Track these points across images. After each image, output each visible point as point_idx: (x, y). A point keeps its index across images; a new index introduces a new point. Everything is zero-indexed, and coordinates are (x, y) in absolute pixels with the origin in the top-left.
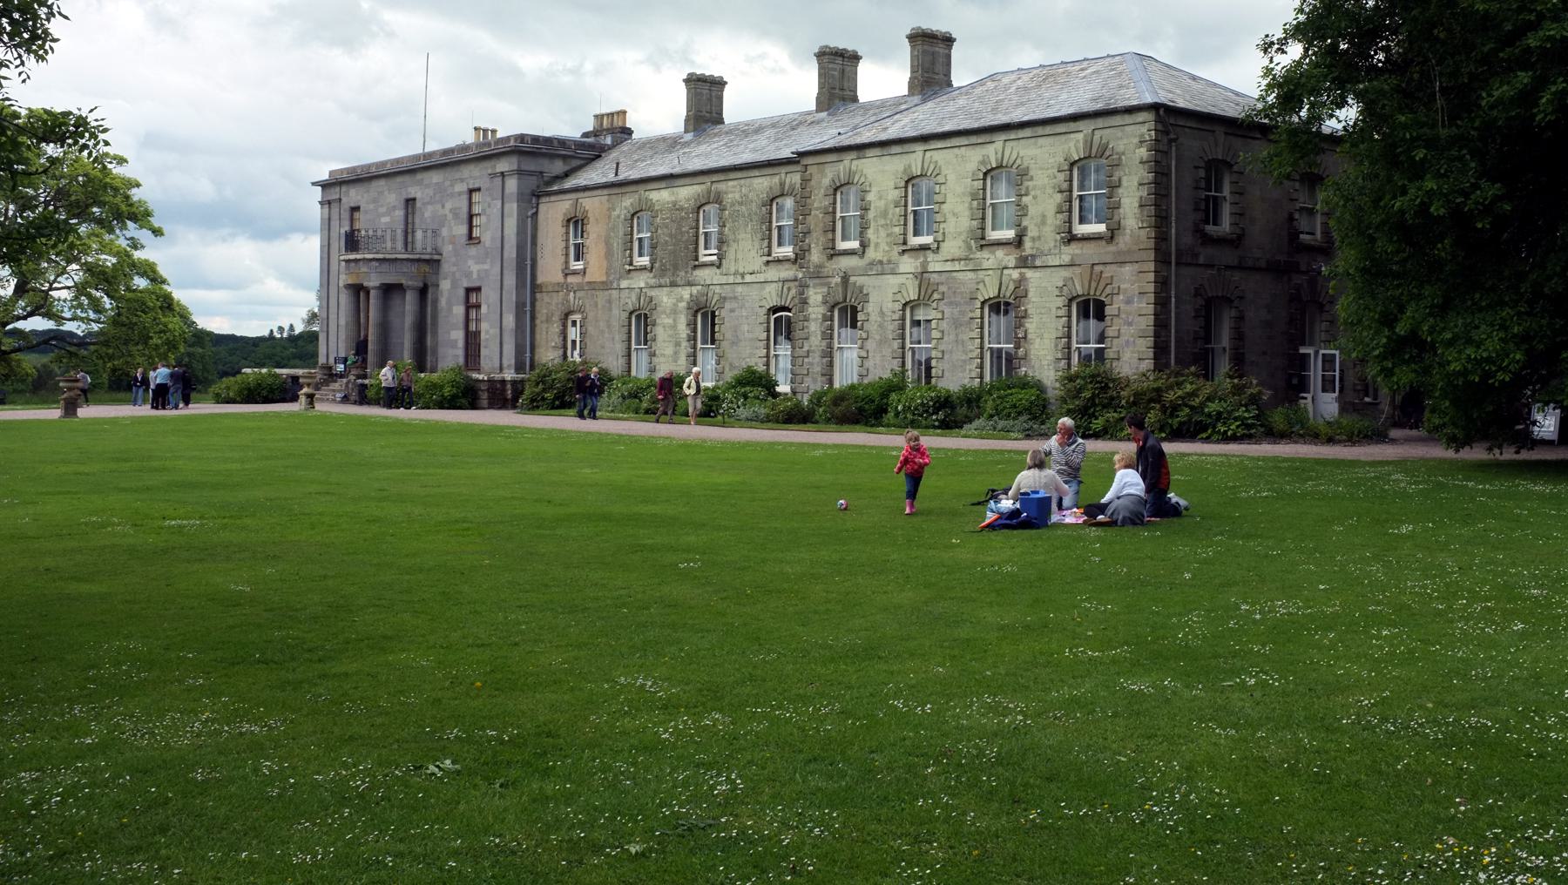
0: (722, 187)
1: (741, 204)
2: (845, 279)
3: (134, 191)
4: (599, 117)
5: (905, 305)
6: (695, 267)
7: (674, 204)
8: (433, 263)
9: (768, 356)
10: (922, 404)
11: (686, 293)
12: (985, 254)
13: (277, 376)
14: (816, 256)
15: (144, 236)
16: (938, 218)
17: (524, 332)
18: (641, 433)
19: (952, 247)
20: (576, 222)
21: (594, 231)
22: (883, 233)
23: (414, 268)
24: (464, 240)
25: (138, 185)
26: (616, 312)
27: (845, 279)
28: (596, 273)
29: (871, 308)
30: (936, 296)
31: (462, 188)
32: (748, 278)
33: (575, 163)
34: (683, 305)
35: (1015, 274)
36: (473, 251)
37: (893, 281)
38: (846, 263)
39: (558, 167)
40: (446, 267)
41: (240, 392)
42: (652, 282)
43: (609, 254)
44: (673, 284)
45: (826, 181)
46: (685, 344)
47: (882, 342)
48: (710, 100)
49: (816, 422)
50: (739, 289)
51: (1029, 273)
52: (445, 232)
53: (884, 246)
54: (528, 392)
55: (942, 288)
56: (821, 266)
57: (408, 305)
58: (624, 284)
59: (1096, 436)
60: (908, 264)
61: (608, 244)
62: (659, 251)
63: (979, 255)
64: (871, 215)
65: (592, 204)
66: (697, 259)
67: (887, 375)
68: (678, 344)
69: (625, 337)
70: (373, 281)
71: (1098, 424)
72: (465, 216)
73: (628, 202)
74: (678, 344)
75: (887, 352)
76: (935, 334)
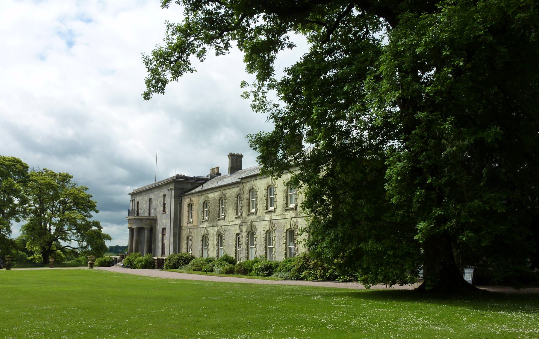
0: (225, 191)
1: (230, 197)
2: (252, 223)
3: (90, 199)
4: (212, 170)
5: (267, 232)
6: (218, 220)
7: (214, 197)
8: (155, 220)
9: (236, 251)
10: (261, 267)
11: (216, 229)
12: (287, 213)
13: (111, 258)
14: (244, 215)
15: (92, 213)
16: (275, 200)
17: (176, 243)
18: (269, 283)
19: (279, 211)
20: (190, 205)
21: (195, 207)
22: (261, 206)
23: (148, 222)
24: (162, 212)
25: (91, 196)
26: (199, 236)
27: (252, 223)
28: (195, 223)
29: (258, 233)
30: (274, 228)
31: (162, 194)
32: (231, 223)
33: (196, 185)
34: (215, 233)
35: (295, 220)
36: (164, 216)
37: (263, 223)
38: (252, 217)
39: (189, 186)
40: (159, 221)
41: (99, 264)
42: (208, 225)
43: (198, 215)
44: (213, 226)
45: (247, 188)
46: (216, 247)
47: (260, 245)
48: (237, 162)
49: (234, 274)
50: (229, 227)
51: (299, 219)
52: (158, 209)
53: (261, 211)
54: (166, 263)
55: (276, 226)
56: (245, 218)
57: (146, 234)
58: (201, 226)
59: (302, 279)
60: (267, 217)
61: (198, 212)
62: (210, 215)
63: (285, 213)
64: (258, 199)
65: (195, 199)
66: (219, 217)
67: (19, 235)
68: (214, 247)
69: (201, 244)
70: (134, 227)
71: (302, 275)
72: (162, 204)
73: (203, 198)
74: (214, 247)
75: (262, 249)
76: (274, 242)
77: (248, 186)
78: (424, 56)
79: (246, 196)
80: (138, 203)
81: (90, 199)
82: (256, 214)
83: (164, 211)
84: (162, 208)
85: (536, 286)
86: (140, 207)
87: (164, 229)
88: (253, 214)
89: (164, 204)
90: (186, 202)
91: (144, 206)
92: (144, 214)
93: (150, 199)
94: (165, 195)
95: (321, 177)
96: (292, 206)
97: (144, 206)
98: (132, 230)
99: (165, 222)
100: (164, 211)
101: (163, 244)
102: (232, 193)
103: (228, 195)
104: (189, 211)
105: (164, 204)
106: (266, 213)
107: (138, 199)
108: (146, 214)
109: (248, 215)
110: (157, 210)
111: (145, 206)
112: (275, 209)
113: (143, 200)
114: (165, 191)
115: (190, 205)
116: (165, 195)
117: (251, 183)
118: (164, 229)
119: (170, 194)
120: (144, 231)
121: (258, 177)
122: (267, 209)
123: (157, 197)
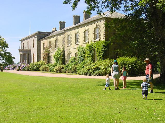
3: (6, 43)
6: (55, 49)
8: (30, 51)
31: (32, 40)
39: (43, 36)
77: (67, 34)
78: (145, 10)
79: (66, 38)
80: (23, 44)
81: (6, 43)
82: (71, 46)
83: (33, 46)
84: (33, 46)
85: (164, 89)
86: (24, 46)
87: (34, 54)
88: (69, 46)
89: (33, 44)
90: (42, 42)
91: (26, 45)
92: (26, 48)
93: (28, 42)
94: (33, 40)
95: (134, 59)
96: (87, 41)
97: (26, 45)
98: (21, 55)
99: (34, 51)
100: (33, 46)
101: (33, 58)
102: (60, 38)
103: (59, 39)
104: (43, 46)
105: (33, 44)
106: (75, 45)
107: (23, 42)
108: (27, 48)
109: (67, 46)
110: (31, 47)
111: (26, 45)
112: (71, 45)
113: (25, 42)
114: (33, 38)
115: (44, 44)
116: (33, 40)
117: (68, 32)
118: (34, 54)
119: (35, 39)
120: (26, 55)
121: (71, 30)
122: (68, 45)
123: (30, 40)
